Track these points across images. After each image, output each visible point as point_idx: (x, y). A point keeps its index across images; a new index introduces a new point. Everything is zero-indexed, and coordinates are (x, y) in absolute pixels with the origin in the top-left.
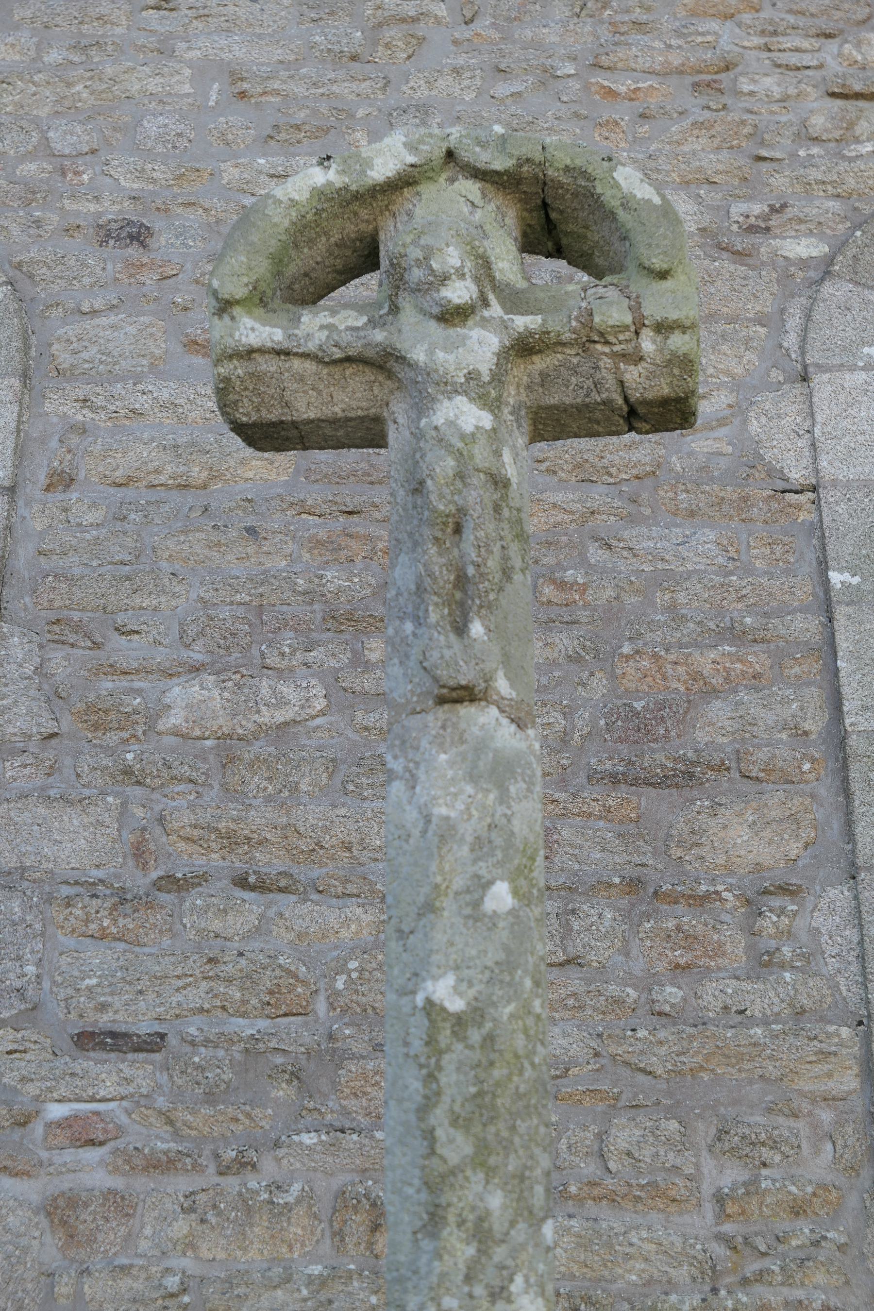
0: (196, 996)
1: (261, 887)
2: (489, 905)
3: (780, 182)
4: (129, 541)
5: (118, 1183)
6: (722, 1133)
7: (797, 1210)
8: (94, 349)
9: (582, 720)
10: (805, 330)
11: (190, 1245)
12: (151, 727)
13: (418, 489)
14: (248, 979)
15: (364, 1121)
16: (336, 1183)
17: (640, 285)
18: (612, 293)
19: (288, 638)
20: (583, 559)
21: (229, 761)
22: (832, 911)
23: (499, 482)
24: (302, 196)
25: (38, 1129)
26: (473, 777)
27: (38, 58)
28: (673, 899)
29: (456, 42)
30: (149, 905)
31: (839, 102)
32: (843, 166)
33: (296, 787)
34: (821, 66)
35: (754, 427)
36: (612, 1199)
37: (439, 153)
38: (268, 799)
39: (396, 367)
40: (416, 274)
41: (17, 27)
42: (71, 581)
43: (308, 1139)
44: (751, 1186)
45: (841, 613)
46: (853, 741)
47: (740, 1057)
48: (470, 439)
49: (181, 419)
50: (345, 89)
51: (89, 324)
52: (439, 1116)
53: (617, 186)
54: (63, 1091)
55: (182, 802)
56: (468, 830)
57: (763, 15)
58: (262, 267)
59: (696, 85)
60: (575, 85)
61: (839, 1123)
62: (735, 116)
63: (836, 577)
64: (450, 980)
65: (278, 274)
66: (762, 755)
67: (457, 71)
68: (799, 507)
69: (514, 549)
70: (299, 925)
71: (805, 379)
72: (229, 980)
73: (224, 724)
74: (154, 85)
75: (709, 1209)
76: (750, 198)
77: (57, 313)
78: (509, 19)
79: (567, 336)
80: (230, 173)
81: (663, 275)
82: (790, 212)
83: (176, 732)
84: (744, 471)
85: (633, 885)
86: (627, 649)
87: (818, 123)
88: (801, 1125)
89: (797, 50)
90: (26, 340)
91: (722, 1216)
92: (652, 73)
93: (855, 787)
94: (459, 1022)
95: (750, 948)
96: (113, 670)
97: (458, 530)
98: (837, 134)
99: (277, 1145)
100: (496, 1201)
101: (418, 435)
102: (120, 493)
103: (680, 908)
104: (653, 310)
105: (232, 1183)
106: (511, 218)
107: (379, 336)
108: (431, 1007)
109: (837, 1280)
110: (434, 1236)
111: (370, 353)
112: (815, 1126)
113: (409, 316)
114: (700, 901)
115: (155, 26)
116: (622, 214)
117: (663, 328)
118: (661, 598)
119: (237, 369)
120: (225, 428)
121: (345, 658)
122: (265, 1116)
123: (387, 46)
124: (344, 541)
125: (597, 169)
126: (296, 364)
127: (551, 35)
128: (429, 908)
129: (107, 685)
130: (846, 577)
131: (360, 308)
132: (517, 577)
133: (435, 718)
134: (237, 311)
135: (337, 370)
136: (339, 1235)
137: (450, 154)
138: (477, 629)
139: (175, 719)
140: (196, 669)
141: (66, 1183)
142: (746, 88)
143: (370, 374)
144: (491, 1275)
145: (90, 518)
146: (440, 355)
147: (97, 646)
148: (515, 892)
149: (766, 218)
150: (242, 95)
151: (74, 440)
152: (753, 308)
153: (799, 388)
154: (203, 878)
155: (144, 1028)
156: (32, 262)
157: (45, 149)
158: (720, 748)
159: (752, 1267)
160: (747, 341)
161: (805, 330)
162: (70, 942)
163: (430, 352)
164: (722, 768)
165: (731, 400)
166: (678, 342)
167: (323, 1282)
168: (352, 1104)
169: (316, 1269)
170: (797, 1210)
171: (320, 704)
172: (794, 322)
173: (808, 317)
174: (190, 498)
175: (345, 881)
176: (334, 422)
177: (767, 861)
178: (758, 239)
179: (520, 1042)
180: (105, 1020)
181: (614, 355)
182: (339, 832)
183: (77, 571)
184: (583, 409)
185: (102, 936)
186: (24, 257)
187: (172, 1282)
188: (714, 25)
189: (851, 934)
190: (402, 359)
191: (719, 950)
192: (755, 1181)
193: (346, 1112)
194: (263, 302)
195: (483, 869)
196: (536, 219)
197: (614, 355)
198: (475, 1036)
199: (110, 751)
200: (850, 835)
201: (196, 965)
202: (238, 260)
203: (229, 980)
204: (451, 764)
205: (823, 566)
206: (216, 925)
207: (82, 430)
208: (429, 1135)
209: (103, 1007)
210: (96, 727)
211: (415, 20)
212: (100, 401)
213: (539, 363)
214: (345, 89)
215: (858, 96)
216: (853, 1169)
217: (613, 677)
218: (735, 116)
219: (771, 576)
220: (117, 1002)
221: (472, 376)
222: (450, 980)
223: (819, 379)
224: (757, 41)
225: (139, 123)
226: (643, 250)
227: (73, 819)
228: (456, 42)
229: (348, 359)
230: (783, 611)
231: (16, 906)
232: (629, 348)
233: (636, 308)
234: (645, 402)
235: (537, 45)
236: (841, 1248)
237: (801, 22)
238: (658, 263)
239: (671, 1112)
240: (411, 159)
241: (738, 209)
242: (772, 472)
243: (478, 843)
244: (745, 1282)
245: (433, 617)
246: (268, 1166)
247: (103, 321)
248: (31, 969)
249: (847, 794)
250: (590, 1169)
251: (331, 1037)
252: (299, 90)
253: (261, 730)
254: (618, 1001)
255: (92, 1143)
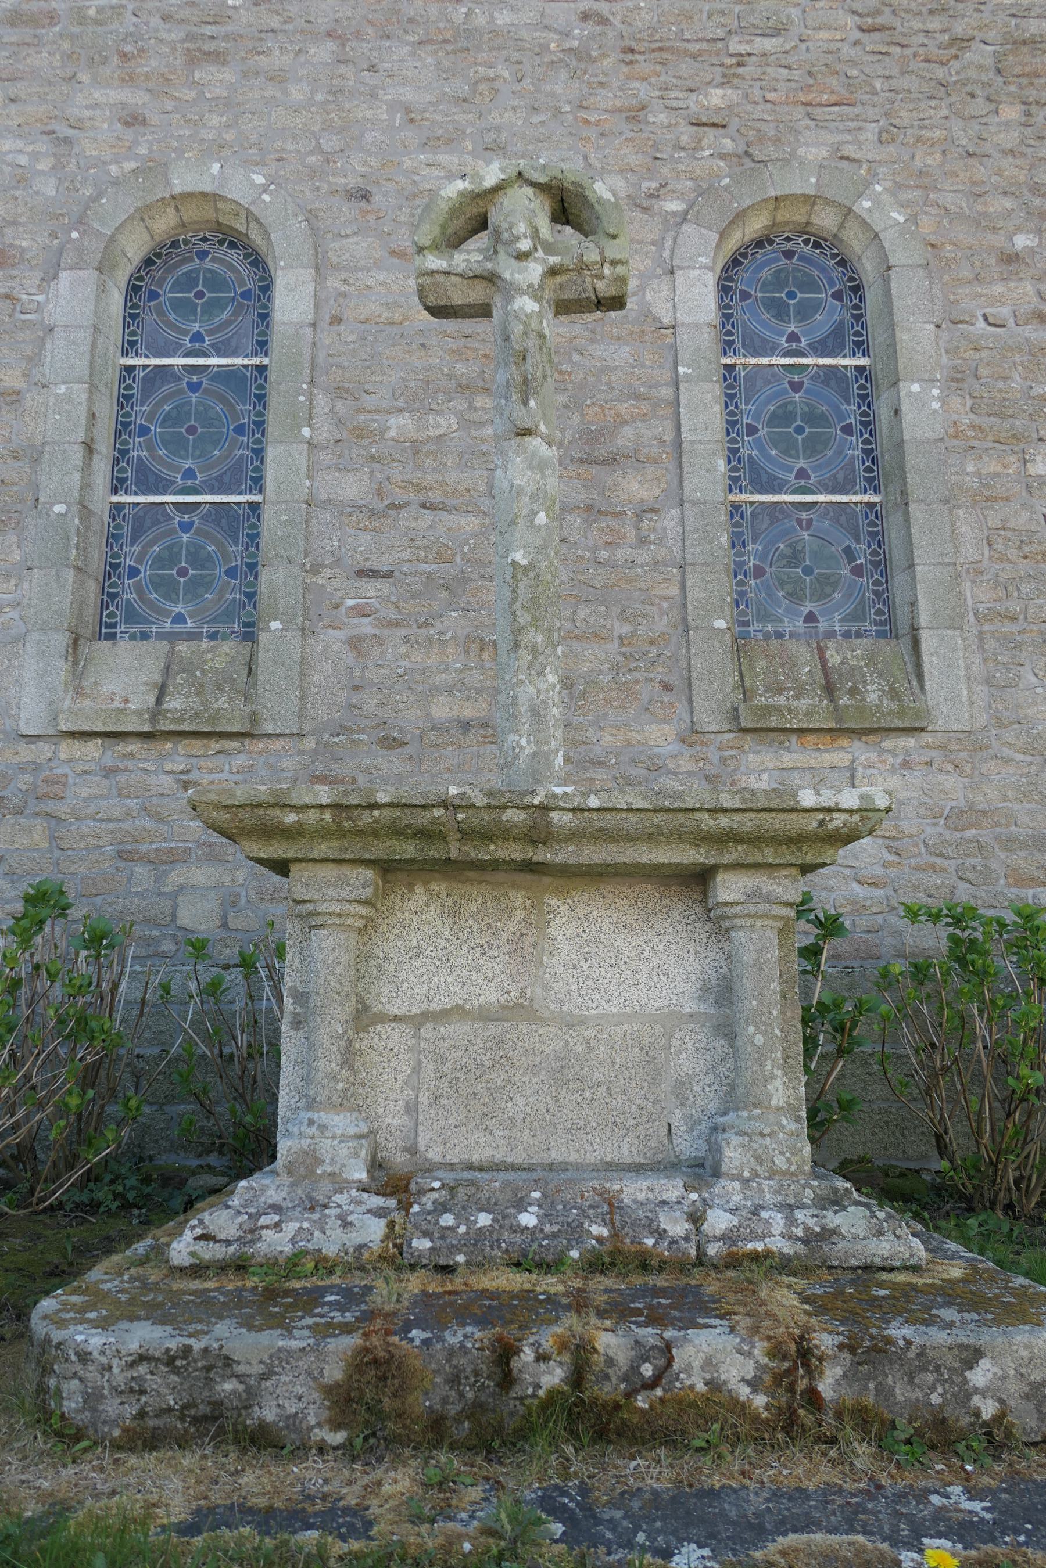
0: (406, 555)
1: (432, 508)
2: (537, 522)
3: (665, 171)
4: (368, 350)
5: (377, 632)
6: (623, 612)
7: (652, 643)
8: (347, 255)
9: (569, 434)
10: (673, 248)
11: (407, 656)
12: (382, 438)
13: (507, 339)
14: (427, 548)
15: (477, 607)
16: (465, 632)
17: (605, 242)
18: (592, 245)
19: (440, 397)
20: (570, 361)
21: (416, 452)
22: (672, 519)
23: (542, 336)
24: (453, 195)
25: (343, 610)
26: (531, 468)
27: (312, 98)
28: (606, 514)
29: (513, 92)
30: (385, 516)
31: (695, 128)
32: (695, 163)
33: (445, 464)
34: (687, 108)
35: (648, 296)
36: (577, 638)
37: (515, 173)
38: (434, 469)
39: (497, 281)
40: (506, 236)
41: (300, 80)
42: (343, 368)
43: (454, 614)
44: (634, 633)
45: (683, 386)
46: (685, 445)
47: (631, 581)
48: (529, 316)
49: (389, 290)
50: (461, 118)
51: (345, 241)
52: (517, 606)
53: (595, 192)
54: (352, 594)
55: (396, 471)
56: (528, 490)
57: (662, 79)
58: (437, 230)
59: (627, 118)
60: (570, 117)
61: (670, 608)
62: (645, 135)
63: (681, 370)
64: (522, 552)
65: (443, 233)
66: (645, 451)
67: (514, 109)
68: (666, 336)
69: (548, 366)
70: (448, 524)
71: (672, 273)
72: (420, 548)
73: (413, 435)
74: (369, 114)
75: (616, 642)
76: (651, 179)
77: (329, 236)
78: (539, 80)
79: (572, 267)
80: (407, 163)
81: (614, 237)
82: (669, 187)
83: (393, 439)
84: (643, 318)
85: (589, 508)
86: (589, 402)
87: (684, 139)
88: (655, 609)
89: (677, 99)
90: (316, 250)
91: (622, 644)
92: (607, 111)
93: (684, 465)
94: (525, 569)
95: (637, 535)
96: (364, 411)
97: (524, 358)
98: (693, 145)
99: (441, 616)
100: (539, 639)
101: (507, 314)
102: (363, 326)
103: (609, 518)
104: (610, 255)
105: (423, 632)
106: (547, 207)
107: (489, 266)
108: (514, 563)
109: (666, 670)
110: (516, 652)
111: (485, 274)
112: (660, 609)
113: (502, 256)
114: (617, 515)
115: (368, 81)
116: (596, 206)
117: (614, 263)
118: (604, 379)
119: (427, 280)
120: (421, 307)
121: (466, 406)
122: (436, 605)
123: (481, 94)
124: (464, 350)
125: (586, 183)
126: (453, 278)
127: (559, 89)
128: (513, 523)
129: (362, 417)
130: (685, 369)
131: (480, 251)
132: (549, 379)
133: (515, 442)
134: (426, 252)
135: (470, 281)
136: (467, 652)
137: (520, 174)
138: (532, 403)
139: (392, 433)
140: (401, 410)
141: (355, 632)
142: (651, 120)
143: (485, 284)
144: (537, 666)
145: (350, 339)
146: (516, 275)
147: (357, 399)
148: (548, 516)
149: (658, 190)
150: (412, 120)
151: (341, 300)
152: (650, 237)
153: (669, 277)
154: (407, 504)
155: (385, 568)
156: (316, 209)
157: (319, 149)
158: (627, 447)
159: (632, 665)
160: (647, 253)
161: (673, 248)
162: (352, 532)
163: (512, 274)
164: (628, 456)
165: (638, 283)
166: (620, 269)
167: (461, 671)
168: (471, 599)
169: (458, 666)
170: (652, 643)
171: (455, 427)
172: (668, 244)
173: (675, 242)
174: (395, 329)
175: (467, 506)
176: (469, 306)
177: (646, 498)
178: (653, 201)
179: (549, 577)
180: (368, 565)
181: (592, 276)
182: (465, 483)
183: (346, 364)
184: (578, 301)
185: (366, 529)
186: (313, 207)
187: (400, 671)
188: (637, 84)
189: (679, 529)
190: (499, 277)
191: (624, 536)
192: (635, 631)
193: (469, 603)
194: (437, 248)
195: (535, 506)
196: (558, 207)
197: (592, 276)
198: (531, 575)
199: (365, 448)
200: (681, 487)
201: (405, 541)
202: (426, 227)
203: (420, 548)
204: (522, 462)
205: (676, 364)
206: (413, 524)
207: (344, 295)
208: (514, 614)
209: (367, 559)
210: (358, 437)
211: (494, 79)
212: (351, 281)
213: (559, 279)
214: (461, 118)
215: (704, 124)
216: (675, 626)
217: (582, 415)
218: (645, 135)
219: (652, 368)
220: (373, 557)
221: (531, 286)
222: (522, 552)
223: (678, 273)
224: (657, 93)
225: (363, 135)
226: (605, 224)
227: (350, 478)
228: (513, 92)
229: (476, 277)
230: (657, 385)
231: (328, 516)
232: (598, 272)
233: (602, 253)
234: (604, 298)
235: (552, 94)
236: (669, 658)
237: (679, 83)
238: (612, 231)
239: (602, 603)
240: (502, 177)
241: (645, 185)
242: (656, 319)
243: (533, 496)
244: (630, 671)
245: (514, 398)
246: (438, 624)
247: (351, 240)
248: (336, 543)
249: (681, 468)
250: (569, 626)
251: (463, 572)
252: (439, 118)
253: (430, 438)
254: (582, 557)
255: (366, 615)
